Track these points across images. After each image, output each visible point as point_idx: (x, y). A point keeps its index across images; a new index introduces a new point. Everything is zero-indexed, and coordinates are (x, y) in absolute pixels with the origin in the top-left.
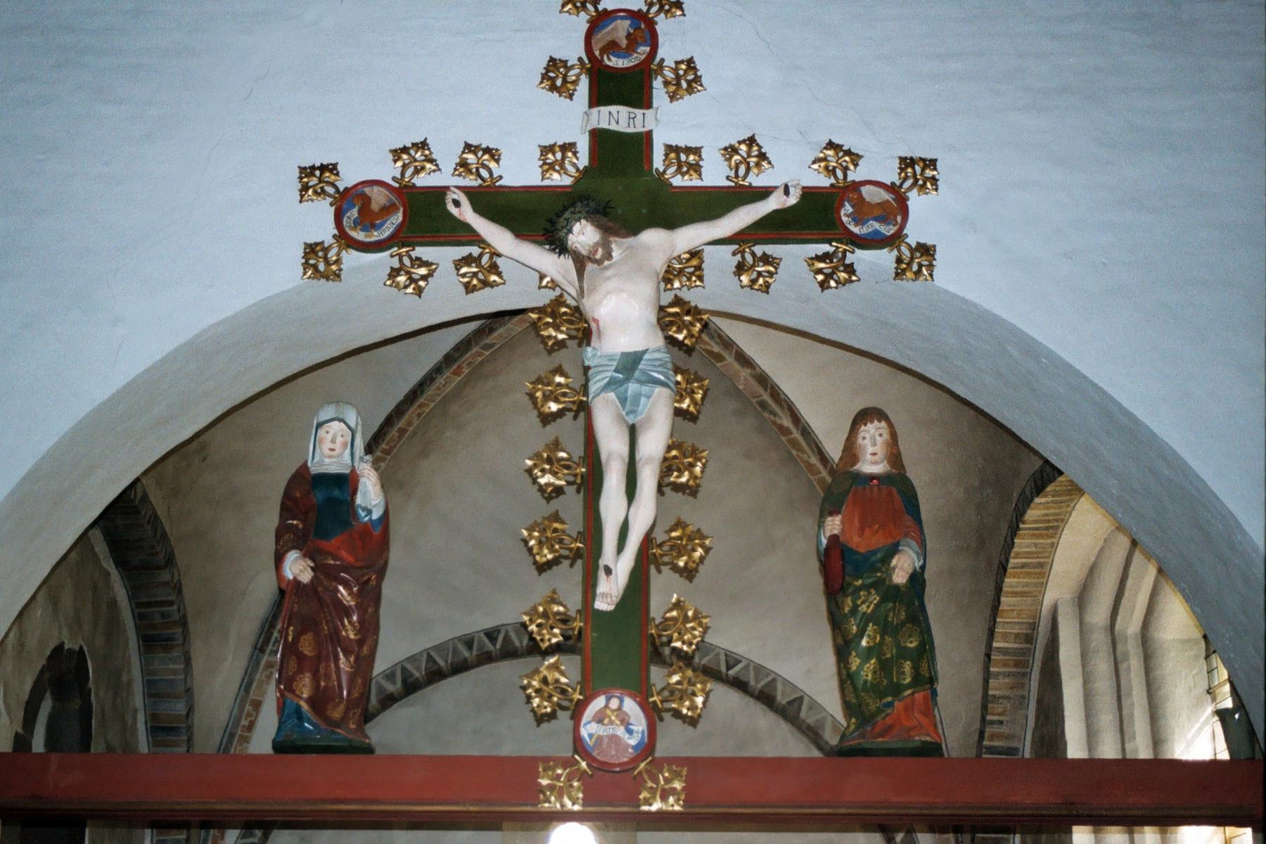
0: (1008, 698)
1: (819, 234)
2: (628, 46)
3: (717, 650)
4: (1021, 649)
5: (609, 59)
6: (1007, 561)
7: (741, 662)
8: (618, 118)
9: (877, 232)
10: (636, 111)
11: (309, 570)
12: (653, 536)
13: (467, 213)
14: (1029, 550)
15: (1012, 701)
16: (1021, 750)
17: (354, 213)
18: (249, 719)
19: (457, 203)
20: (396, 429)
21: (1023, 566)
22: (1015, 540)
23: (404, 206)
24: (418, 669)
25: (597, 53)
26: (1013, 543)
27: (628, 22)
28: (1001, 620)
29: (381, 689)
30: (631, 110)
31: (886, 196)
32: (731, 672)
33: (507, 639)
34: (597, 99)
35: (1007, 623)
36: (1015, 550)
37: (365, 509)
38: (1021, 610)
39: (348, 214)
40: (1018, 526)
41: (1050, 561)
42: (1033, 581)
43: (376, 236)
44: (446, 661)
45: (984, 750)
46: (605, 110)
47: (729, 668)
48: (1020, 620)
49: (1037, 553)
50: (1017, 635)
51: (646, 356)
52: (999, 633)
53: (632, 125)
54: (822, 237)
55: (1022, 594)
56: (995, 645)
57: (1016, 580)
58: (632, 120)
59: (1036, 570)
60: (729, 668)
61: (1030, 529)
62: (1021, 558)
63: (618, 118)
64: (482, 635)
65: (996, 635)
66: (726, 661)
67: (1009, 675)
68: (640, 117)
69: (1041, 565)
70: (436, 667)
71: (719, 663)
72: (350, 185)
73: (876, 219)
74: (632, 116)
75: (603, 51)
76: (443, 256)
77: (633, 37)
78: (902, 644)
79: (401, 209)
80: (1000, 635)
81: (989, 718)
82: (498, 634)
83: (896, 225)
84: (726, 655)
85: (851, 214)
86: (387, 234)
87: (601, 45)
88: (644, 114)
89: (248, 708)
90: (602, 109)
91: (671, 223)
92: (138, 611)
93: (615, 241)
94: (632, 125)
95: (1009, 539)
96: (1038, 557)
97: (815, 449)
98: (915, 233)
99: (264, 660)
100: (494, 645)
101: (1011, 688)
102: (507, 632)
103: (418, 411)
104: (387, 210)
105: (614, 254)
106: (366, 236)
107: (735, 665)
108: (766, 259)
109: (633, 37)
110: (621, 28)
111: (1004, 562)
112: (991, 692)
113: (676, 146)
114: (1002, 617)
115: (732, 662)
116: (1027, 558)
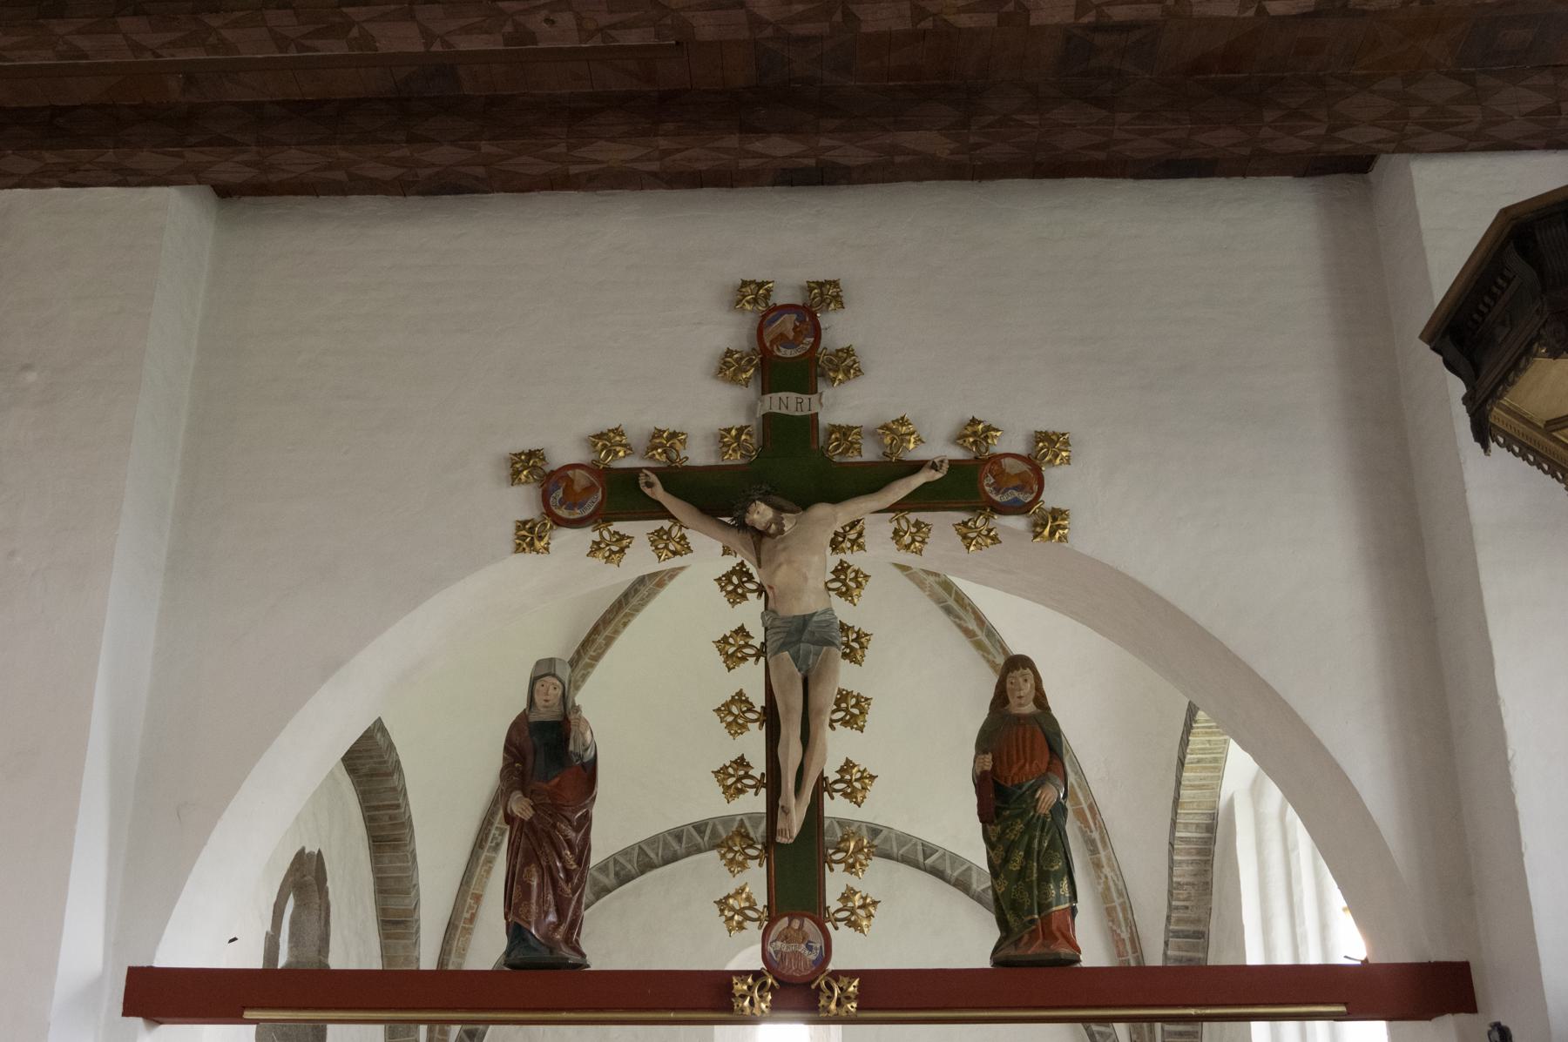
0: (1193, 884)
1: (965, 503)
2: (795, 338)
3: (914, 840)
4: (1203, 838)
5: (778, 349)
6: (1184, 757)
7: (937, 851)
8: (788, 403)
9: (1016, 500)
10: (803, 396)
11: (530, 809)
12: (825, 776)
13: (659, 493)
14: (1203, 746)
15: (1196, 887)
16: (1207, 932)
17: (560, 493)
18: (470, 912)
19: (650, 485)
20: (604, 637)
21: (1199, 761)
22: (1190, 738)
23: (602, 486)
24: (630, 861)
25: (768, 344)
26: (1188, 741)
27: (794, 317)
28: (1182, 811)
29: (595, 882)
30: (799, 395)
31: (1022, 467)
32: (929, 861)
33: (714, 833)
34: (767, 388)
35: (1188, 814)
36: (1190, 747)
37: (576, 754)
38: (1200, 802)
39: (554, 495)
40: (1191, 725)
41: (1224, 756)
42: (1209, 774)
43: (577, 514)
44: (657, 855)
45: (1171, 934)
46: (776, 396)
47: (925, 859)
48: (1200, 811)
49: (1211, 749)
50: (1198, 825)
51: (815, 619)
52: (1180, 823)
53: (799, 409)
54: (967, 505)
55: (1200, 787)
56: (1177, 834)
57: (1192, 774)
58: (799, 405)
59: (1212, 765)
60: (926, 858)
61: (1203, 727)
62: (1197, 754)
63: (788, 403)
64: (690, 827)
65: (1178, 825)
66: (923, 850)
67: (1192, 862)
68: (806, 401)
69: (1216, 760)
70: (647, 859)
71: (916, 852)
72: (556, 468)
73: (1016, 488)
74: (800, 400)
75: (772, 342)
76: (639, 530)
77: (798, 329)
78: (1045, 868)
79: (600, 490)
80: (1182, 825)
81: (1174, 903)
82: (706, 827)
83: (1033, 493)
84: (923, 845)
85: (992, 484)
86: (588, 512)
87: (772, 337)
88: (810, 399)
89: (469, 901)
90: (773, 395)
91: (836, 498)
92: (368, 814)
93: (787, 517)
94: (799, 409)
95: (1185, 737)
96: (1213, 753)
97: (1000, 650)
98: (1050, 499)
99: (483, 858)
100: (703, 838)
101: (1195, 875)
102: (714, 826)
103: (623, 621)
104: (590, 489)
105: (786, 529)
106: (570, 514)
107: (931, 855)
108: (918, 524)
109: (798, 329)
110: (788, 323)
111: (1182, 757)
112: (1175, 879)
113: (839, 426)
114: (1181, 809)
115: (928, 852)
116: (1202, 754)
